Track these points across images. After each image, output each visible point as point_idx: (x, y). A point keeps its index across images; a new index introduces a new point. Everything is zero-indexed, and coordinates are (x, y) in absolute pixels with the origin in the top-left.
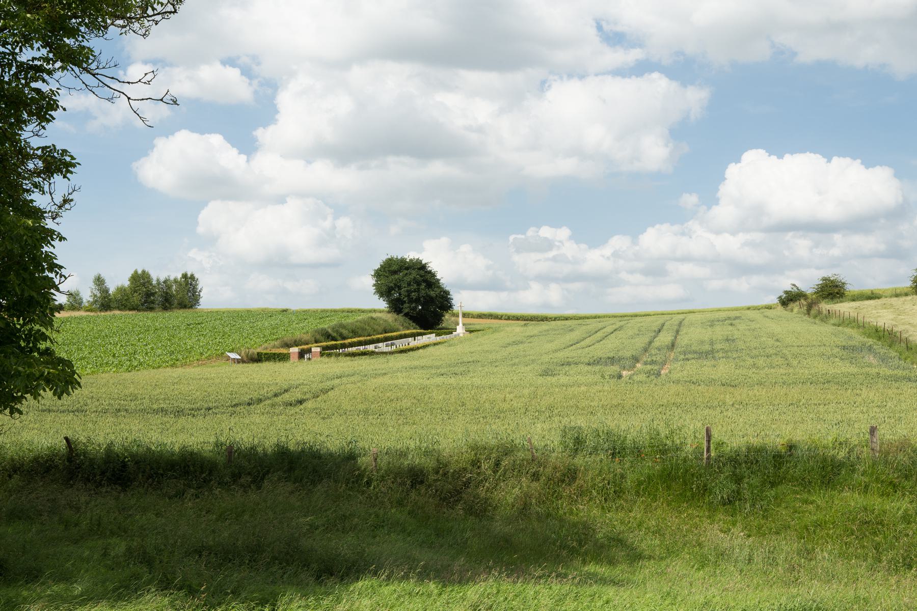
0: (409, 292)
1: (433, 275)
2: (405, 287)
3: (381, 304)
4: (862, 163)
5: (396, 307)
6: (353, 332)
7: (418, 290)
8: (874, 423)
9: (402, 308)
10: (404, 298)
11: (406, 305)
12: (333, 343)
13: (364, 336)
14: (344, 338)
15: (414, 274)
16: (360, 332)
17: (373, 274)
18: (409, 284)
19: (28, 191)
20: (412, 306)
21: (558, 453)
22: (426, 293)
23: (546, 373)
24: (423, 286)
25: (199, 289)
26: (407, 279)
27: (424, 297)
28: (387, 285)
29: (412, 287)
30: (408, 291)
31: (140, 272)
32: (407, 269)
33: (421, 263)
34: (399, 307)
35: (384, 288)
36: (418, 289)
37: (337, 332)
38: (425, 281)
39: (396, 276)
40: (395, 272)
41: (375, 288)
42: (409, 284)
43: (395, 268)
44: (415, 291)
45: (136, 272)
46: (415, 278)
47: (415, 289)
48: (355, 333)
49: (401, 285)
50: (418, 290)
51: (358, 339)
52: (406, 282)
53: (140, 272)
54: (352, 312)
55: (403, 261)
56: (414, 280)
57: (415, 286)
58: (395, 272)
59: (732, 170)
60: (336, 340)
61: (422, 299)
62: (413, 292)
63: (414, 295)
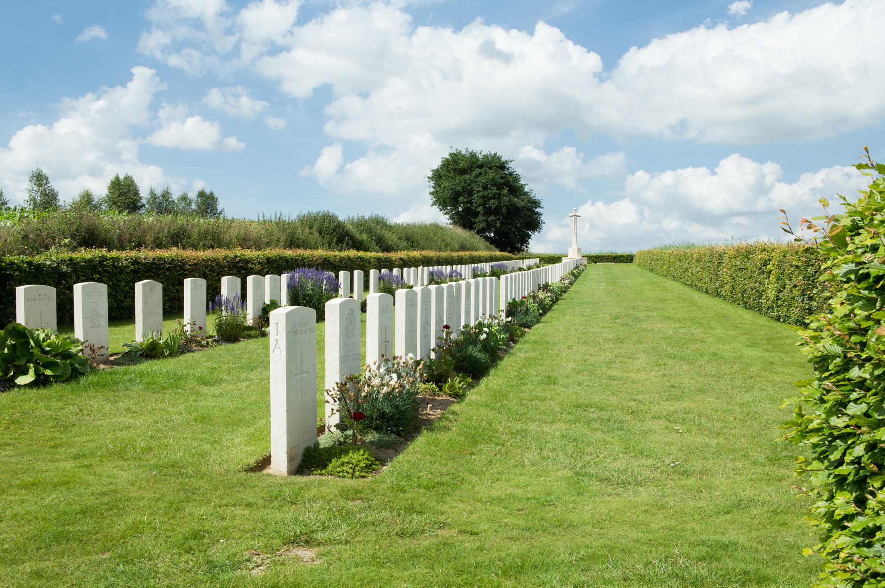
0: (486, 199)
1: (516, 179)
2: (479, 191)
3: (443, 219)
5: (465, 220)
6: (407, 239)
7: (497, 197)
9: (474, 223)
10: (477, 207)
11: (480, 218)
12: (353, 253)
14: (388, 249)
15: (491, 174)
16: (422, 243)
18: (485, 188)
20: (489, 219)
22: (510, 200)
23: (649, 317)
25: (220, 210)
26: (482, 180)
27: (507, 206)
28: (452, 189)
30: (483, 197)
31: (122, 178)
32: (481, 167)
33: (500, 160)
34: (470, 221)
35: (448, 193)
37: (370, 231)
38: (507, 184)
39: (466, 177)
40: (463, 171)
42: (485, 188)
43: (462, 165)
44: (494, 198)
45: (117, 178)
46: (493, 179)
47: (494, 195)
48: (412, 242)
49: (472, 189)
50: (497, 197)
51: (417, 254)
52: (481, 184)
53: (122, 178)
55: (473, 156)
56: (492, 181)
58: (463, 171)
60: (366, 249)
61: (504, 209)
62: (491, 198)
63: (493, 204)
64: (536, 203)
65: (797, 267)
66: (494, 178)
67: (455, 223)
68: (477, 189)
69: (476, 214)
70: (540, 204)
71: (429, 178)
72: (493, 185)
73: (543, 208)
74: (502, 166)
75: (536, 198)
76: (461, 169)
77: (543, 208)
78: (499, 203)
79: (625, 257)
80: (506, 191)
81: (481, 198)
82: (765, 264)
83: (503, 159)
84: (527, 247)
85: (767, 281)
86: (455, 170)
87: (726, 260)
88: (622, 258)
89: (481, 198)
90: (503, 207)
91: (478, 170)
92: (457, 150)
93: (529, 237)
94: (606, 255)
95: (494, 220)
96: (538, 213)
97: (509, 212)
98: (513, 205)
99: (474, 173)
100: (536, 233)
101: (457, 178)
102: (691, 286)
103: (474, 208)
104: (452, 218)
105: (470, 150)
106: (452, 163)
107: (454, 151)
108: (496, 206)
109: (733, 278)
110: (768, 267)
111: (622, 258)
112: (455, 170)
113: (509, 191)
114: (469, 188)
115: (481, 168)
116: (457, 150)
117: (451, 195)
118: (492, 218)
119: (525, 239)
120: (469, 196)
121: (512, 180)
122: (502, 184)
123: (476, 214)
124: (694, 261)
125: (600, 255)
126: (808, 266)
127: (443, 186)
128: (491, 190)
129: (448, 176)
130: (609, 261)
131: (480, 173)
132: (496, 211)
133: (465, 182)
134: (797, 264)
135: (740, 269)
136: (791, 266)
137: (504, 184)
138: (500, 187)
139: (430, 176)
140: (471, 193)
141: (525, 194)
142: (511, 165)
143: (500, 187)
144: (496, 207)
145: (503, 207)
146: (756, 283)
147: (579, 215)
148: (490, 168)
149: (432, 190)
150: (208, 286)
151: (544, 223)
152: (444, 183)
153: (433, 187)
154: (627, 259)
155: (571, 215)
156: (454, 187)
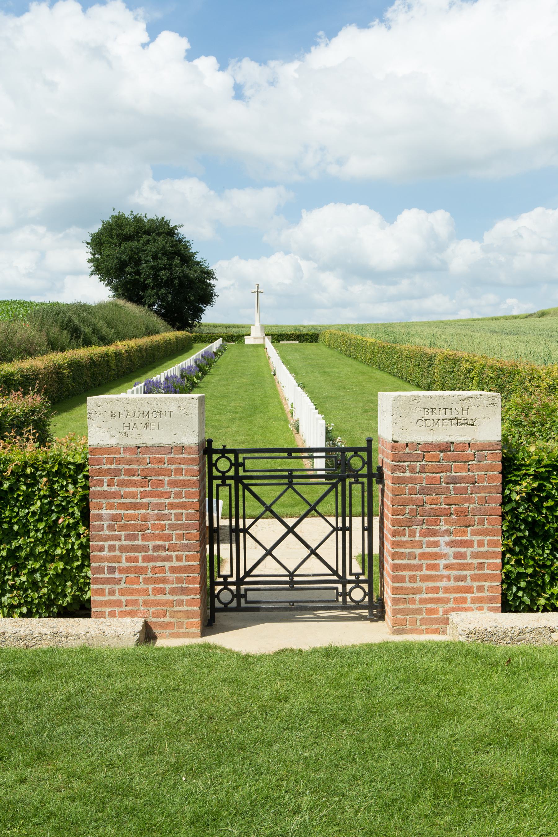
0: (156, 270)
4: (187, 51)
8: (140, 422)
9: (143, 297)
11: (150, 292)
13: (136, 337)
15: (161, 241)
17: (89, 241)
19: (320, 38)
20: (160, 293)
21: (55, 454)
22: (183, 271)
24: (177, 261)
26: (152, 248)
27: (179, 278)
29: (160, 261)
30: (152, 268)
32: (148, 232)
34: (138, 295)
35: (114, 263)
36: (171, 265)
38: (178, 253)
39: (133, 244)
40: (128, 238)
41: (91, 264)
43: (128, 230)
44: (165, 269)
46: (164, 247)
47: (164, 265)
52: (150, 254)
54: (475, 320)
55: (138, 220)
56: (162, 250)
57: (165, 261)
58: (128, 238)
59: (203, 58)
61: (176, 281)
62: (161, 269)
63: (164, 275)
64: (209, 274)
65: (491, 378)
66: (164, 246)
67: (119, 296)
68: (146, 259)
69: (145, 287)
70: (213, 275)
71: (88, 244)
72: (163, 254)
73: (217, 279)
74: (171, 232)
75: (210, 269)
76: (125, 235)
77: (217, 279)
78: (171, 274)
79: (309, 335)
80: (178, 261)
81: (150, 269)
82: (469, 371)
83: (172, 224)
84: (199, 323)
85: (471, 384)
86: (118, 235)
87: (436, 362)
88: (306, 337)
89: (150, 269)
90: (175, 278)
91: (146, 237)
92: (119, 212)
93: (202, 311)
94: (289, 333)
95: (165, 294)
96: (210, 285)
97: (181, 284)
98: (186, 276)
99: (142, 240)
100: (209, 307)
101: (122, 245)
102: (401, 378)
103: (142, 279)
104: (115, 289)
105: (135, 213)
106: (115, 227)
107: (116, 213)
108: (168, 277)
109: (443, 378)
110: (471, 374)
111: (306, 337)
112: (118, 235)
113: (181, 260)
114: (136, 256)
115: (150, 235)
116: (119, 212)
117: (116, 264)
118: (163, 291)
119: (198, 313)
120: (136, 266)
121: (183, 249)
122: (173, 253)
123: (145, 287)
124: (404, 356)
125: (283, 333)
126: (499, 378)
127: (105, 253)
128: (162, 259)
129: (111, 242)
130: (292, 340)
131: (148, 241)
132: (169, 283)
133: (131, 251)
134: (491, 375)
135: (449, 372)
136: (488, 376)
137: (175, 253)
138: (171, 256)
139: (89, 241)
140: (138, 262)
141: (198, 263)
142: (180, 230)
143: (171, 256)
144: (167, 280)
145: (175, 278)
146: (462, 384)
147: (262, 290)
148: (159, 234)
149: (90, 256)
150: (377, 431)
151: (218, 296)
152: (107, 251)
153: (91, 253)
154: (311, 338)
155: (253, 290)
156: (119, 256)
